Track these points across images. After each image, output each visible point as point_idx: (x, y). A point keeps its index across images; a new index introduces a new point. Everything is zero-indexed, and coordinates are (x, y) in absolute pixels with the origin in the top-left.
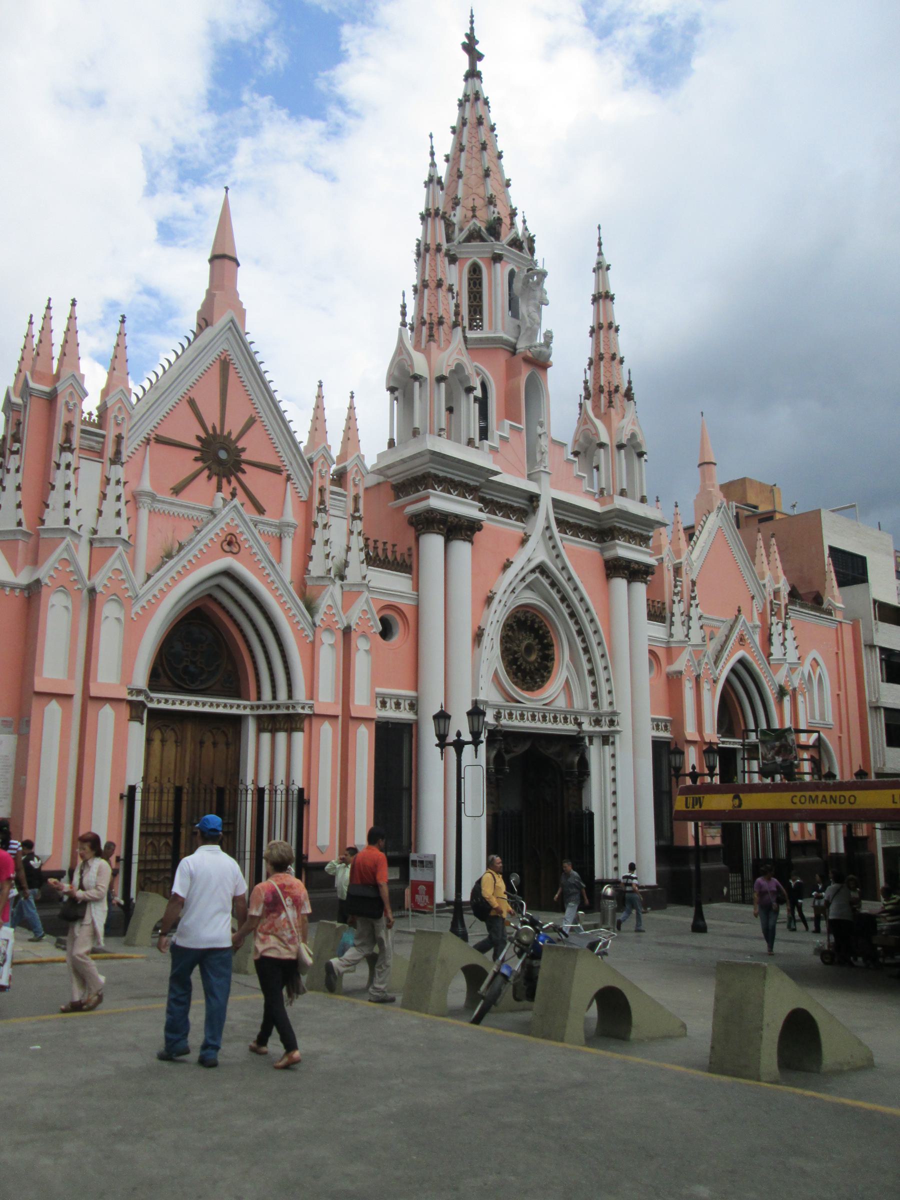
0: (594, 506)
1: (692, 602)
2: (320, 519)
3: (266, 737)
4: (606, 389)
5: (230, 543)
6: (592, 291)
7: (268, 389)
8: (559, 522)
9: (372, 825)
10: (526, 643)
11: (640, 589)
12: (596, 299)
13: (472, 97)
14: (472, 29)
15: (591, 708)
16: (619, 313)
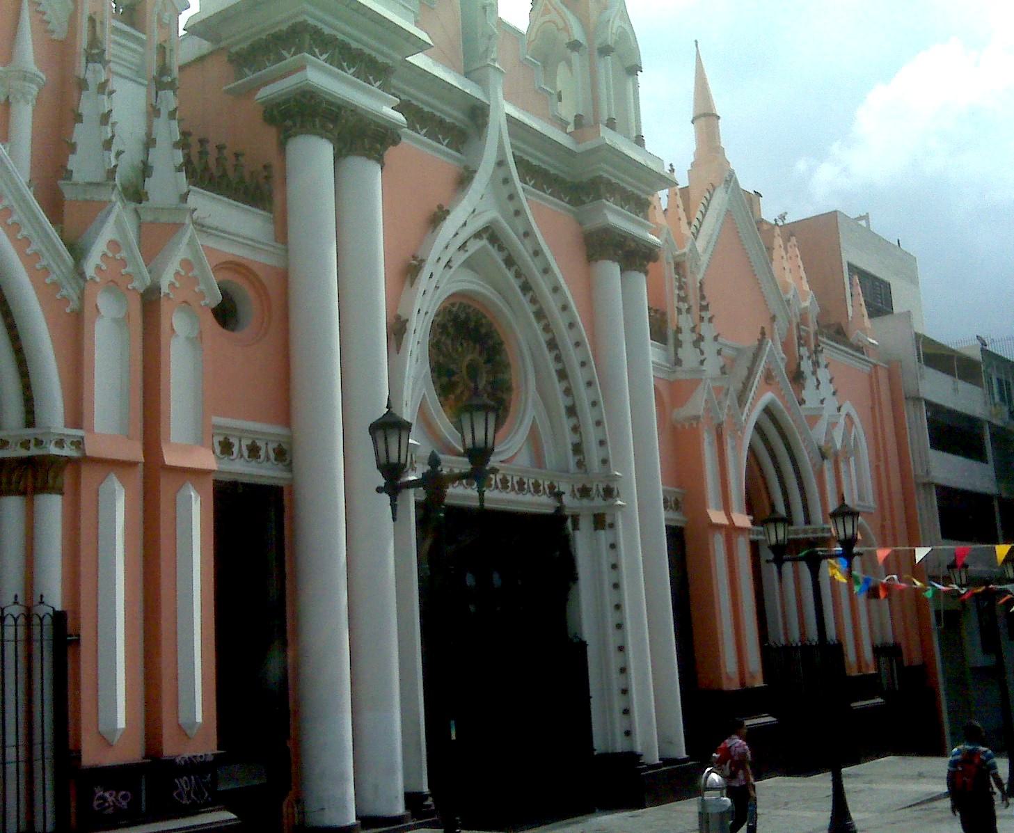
1: (703, 314)
2: (94, 73)
8: (519, 162)
10: (469, 357)
11: (641, 282)
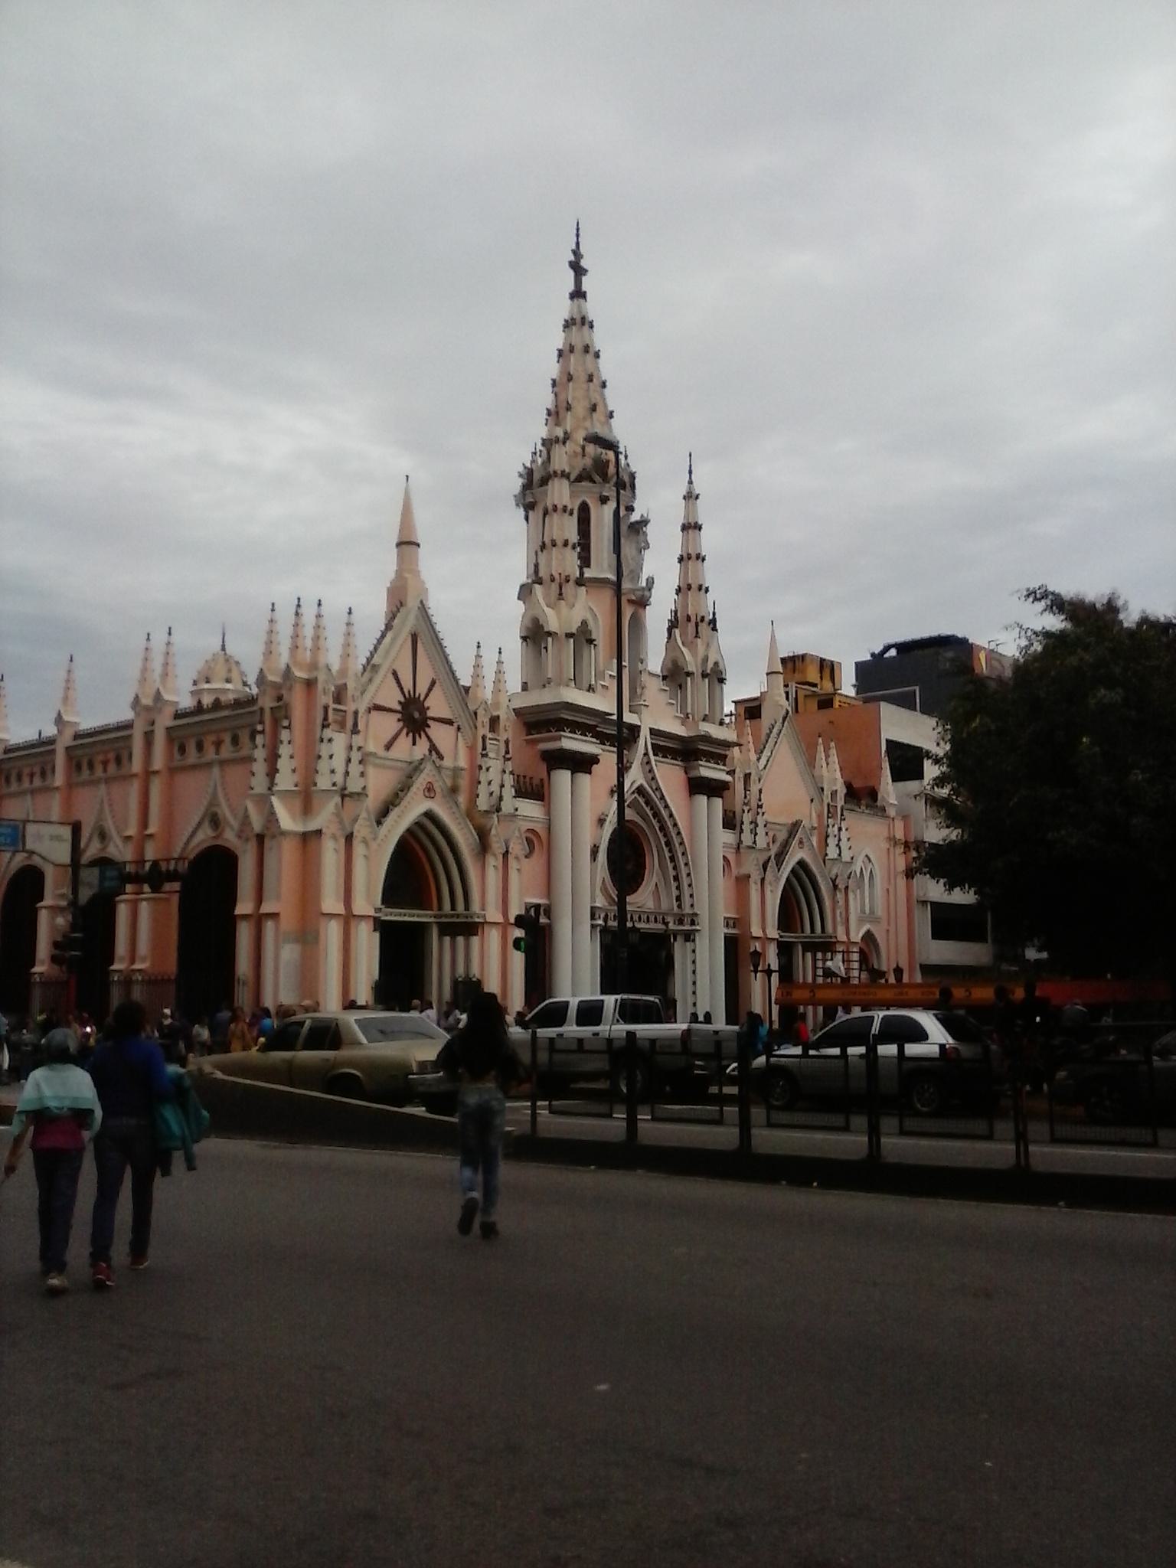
0: (680, 730)
2: (480, 761)
3: (447, 939)
4: (693, 619)
5: (429, 790)
6: (681, 521)
7: (444, 652)
9: (376, 976)
11: (718, 803)
12: (685, 528)
13: (578, 321)
14: (578, 244)
16: (708, 541)
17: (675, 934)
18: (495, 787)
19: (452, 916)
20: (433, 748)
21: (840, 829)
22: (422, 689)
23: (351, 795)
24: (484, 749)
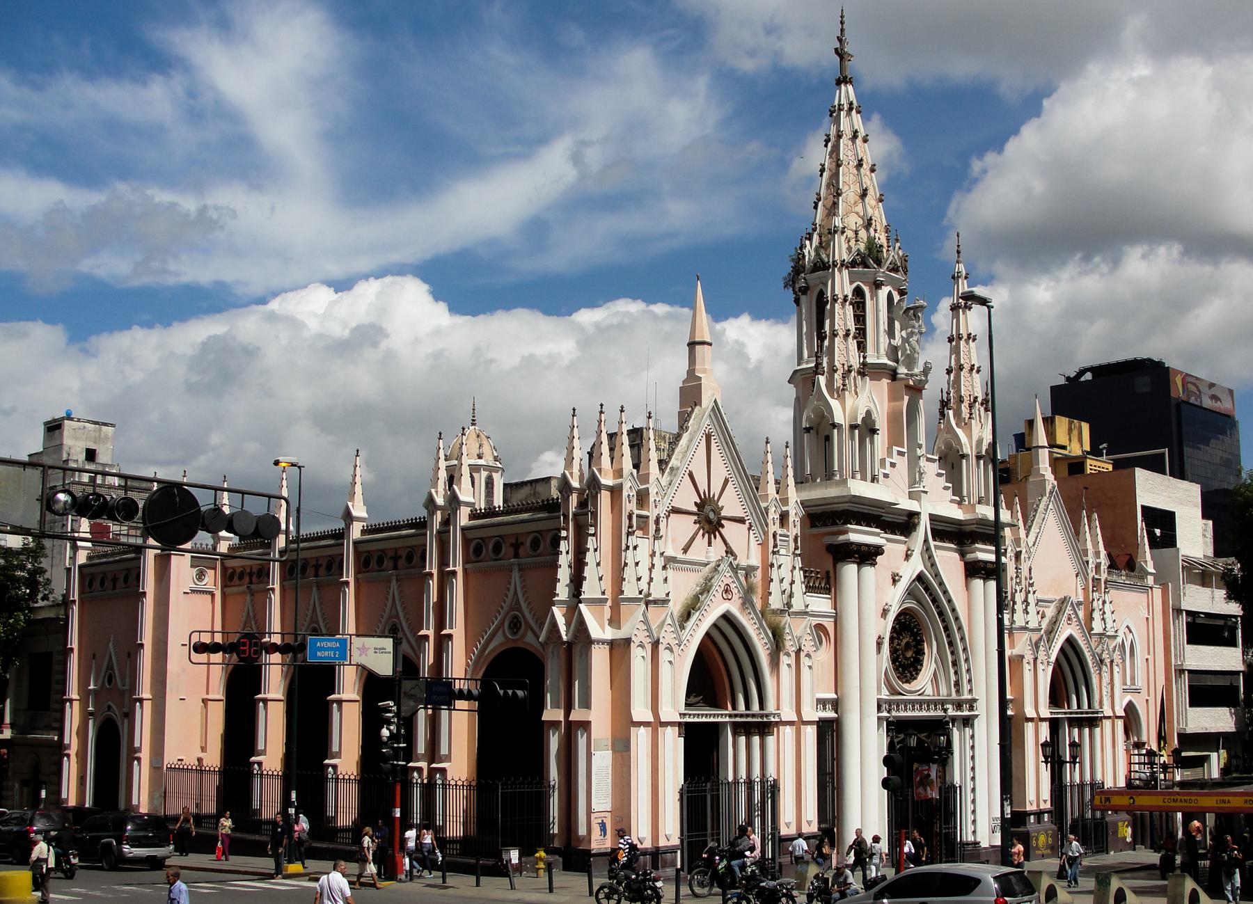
0: (957, 513)
2: (771, 558)
10: (905, 641)
15: (954, 696)
17: (954, 719)
18: (786, 585)
19: (747, 716)
20: (729, 551)
21: (1104, 602)
22: (715, 490)
23: (655, 602)
24: (775, 546)
